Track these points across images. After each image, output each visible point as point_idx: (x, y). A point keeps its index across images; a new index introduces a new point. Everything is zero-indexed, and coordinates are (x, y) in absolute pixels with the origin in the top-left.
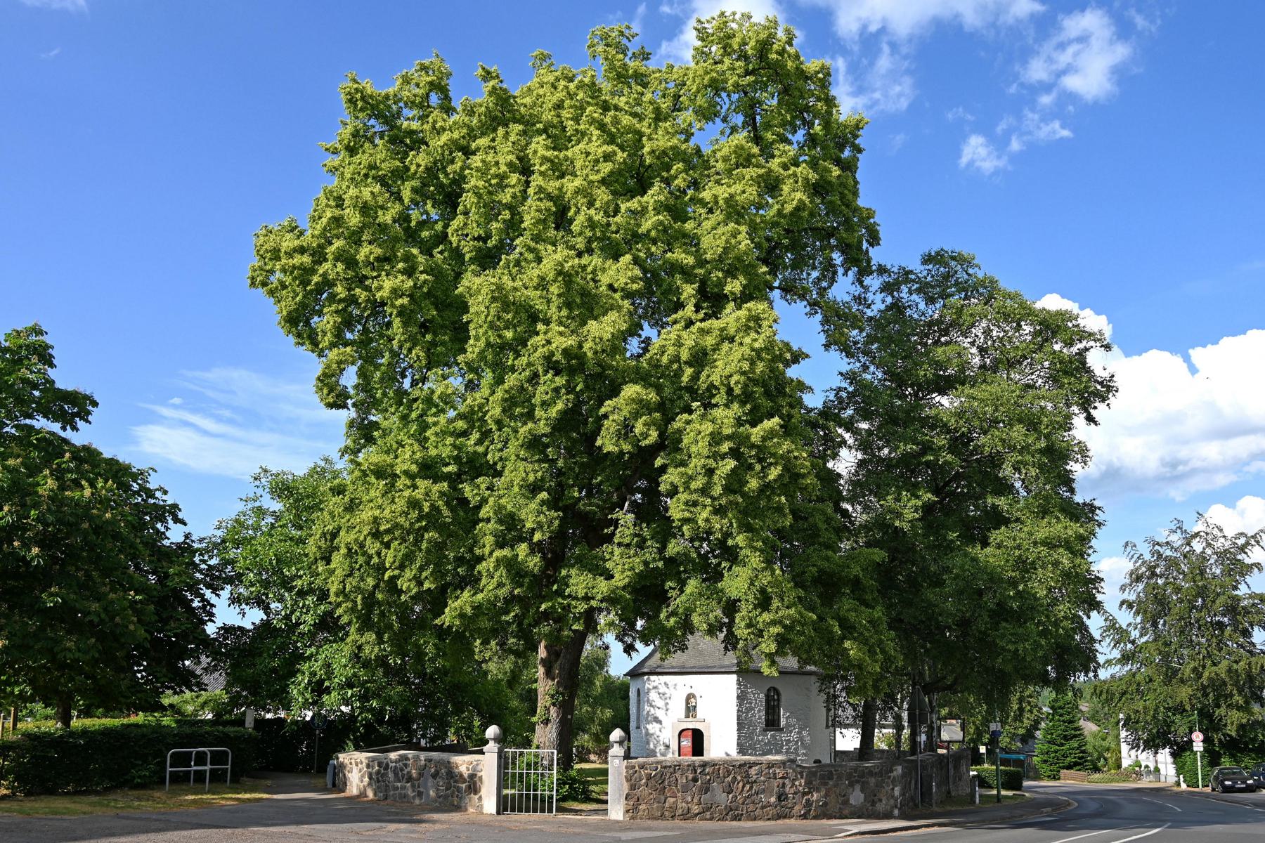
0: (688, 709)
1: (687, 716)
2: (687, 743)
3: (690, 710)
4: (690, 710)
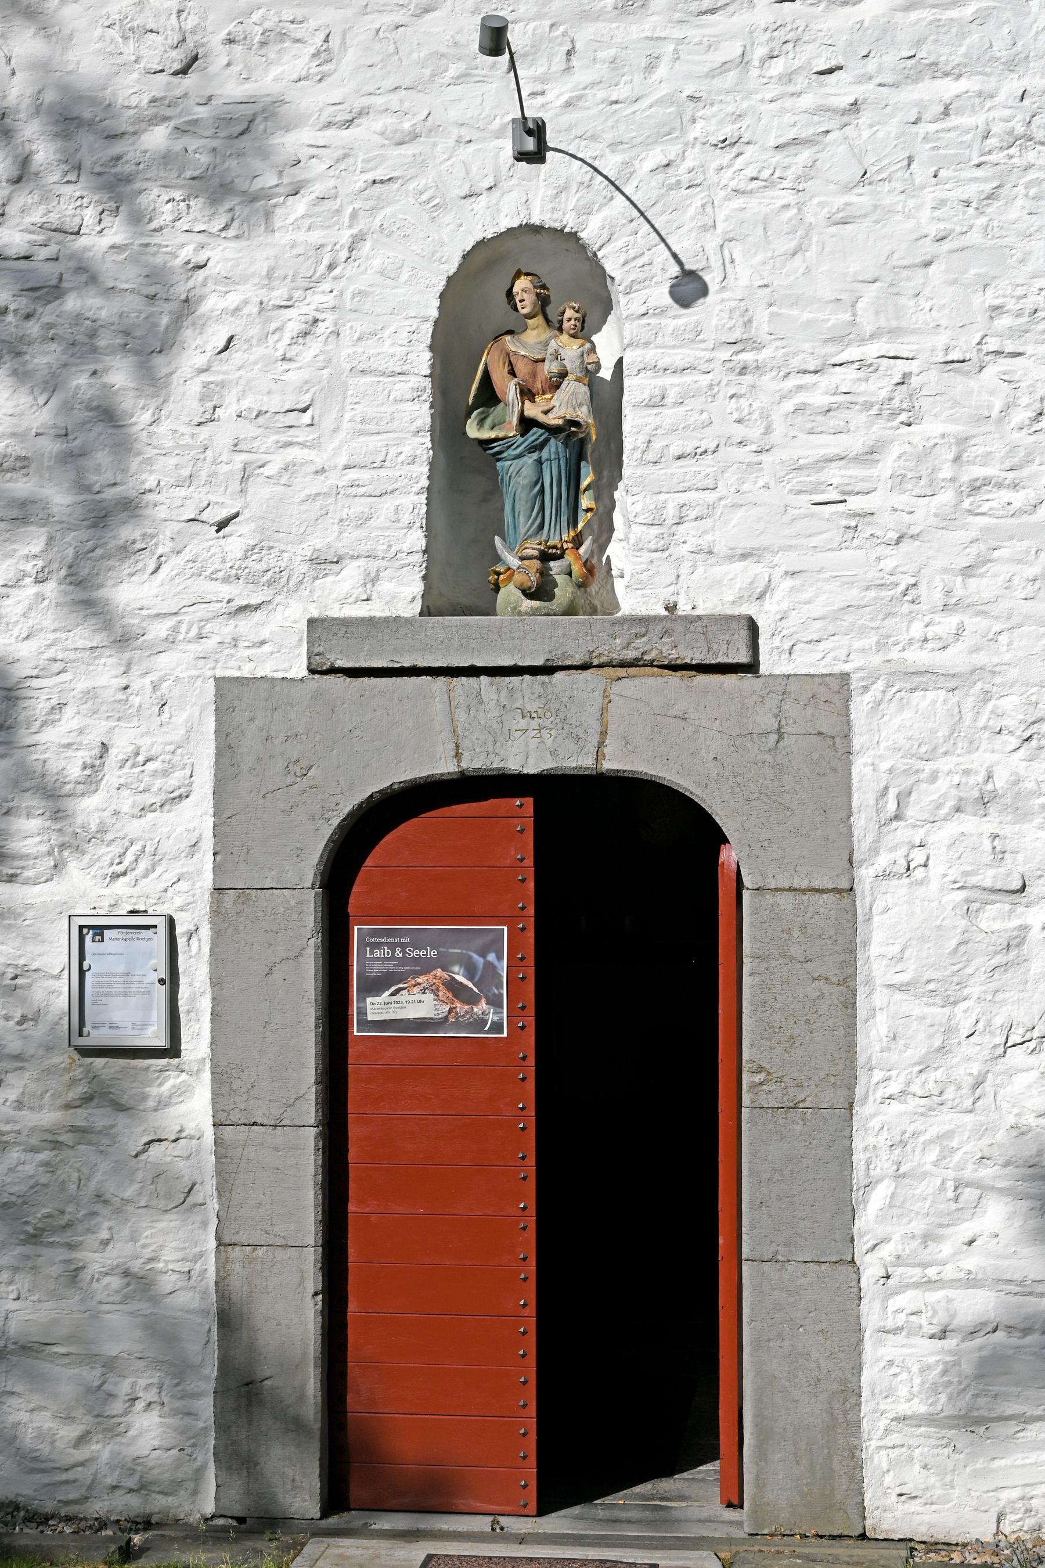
0: (463, 470)
1: (460, 581)
2: (452, 988)
3: (518, 430)
4: (518, 430)
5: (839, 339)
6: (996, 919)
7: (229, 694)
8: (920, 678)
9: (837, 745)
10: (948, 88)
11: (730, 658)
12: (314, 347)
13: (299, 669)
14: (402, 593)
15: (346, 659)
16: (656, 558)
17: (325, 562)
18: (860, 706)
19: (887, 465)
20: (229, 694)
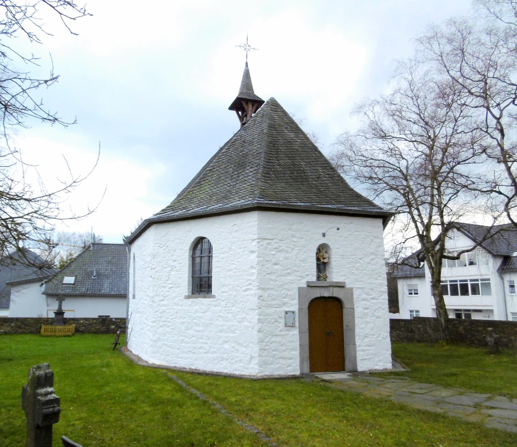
5: (351, 256)
6: (366, 311)
7: (300, 289)
8: (359, 288)
9: (352, 294)
10: (359, 233)
11: (341, 286)
12: (305, 254)
13: (305, 286)
14: (314, 279)
15: (310, 286)
16: (335, 275)
17: (307, 275)
18: (354, 290)
19: (355, 268)
20: (300, 289)
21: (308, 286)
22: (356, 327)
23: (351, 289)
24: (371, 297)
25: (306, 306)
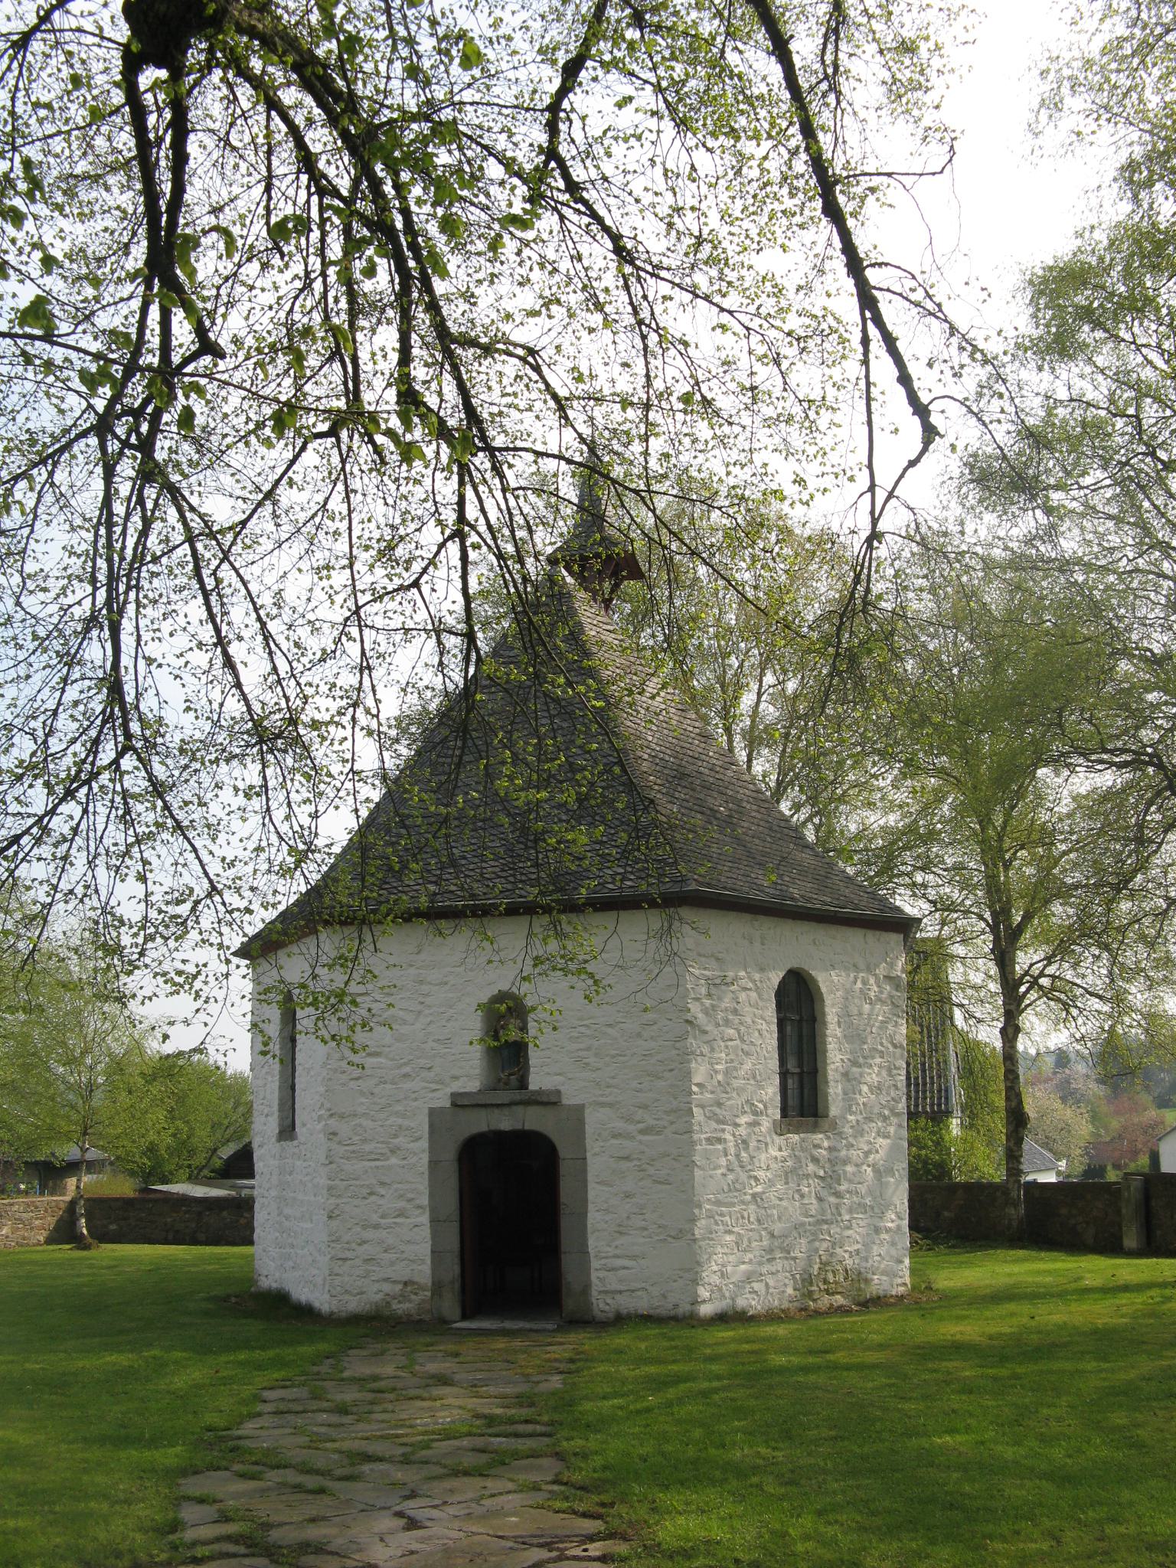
15: (460, 1103)
18: (587, 1111)
21: (454, 1105)
22: (591, 1207)
23: (580, 1108)
24: (641, 1126)
25: (450, 1154)
